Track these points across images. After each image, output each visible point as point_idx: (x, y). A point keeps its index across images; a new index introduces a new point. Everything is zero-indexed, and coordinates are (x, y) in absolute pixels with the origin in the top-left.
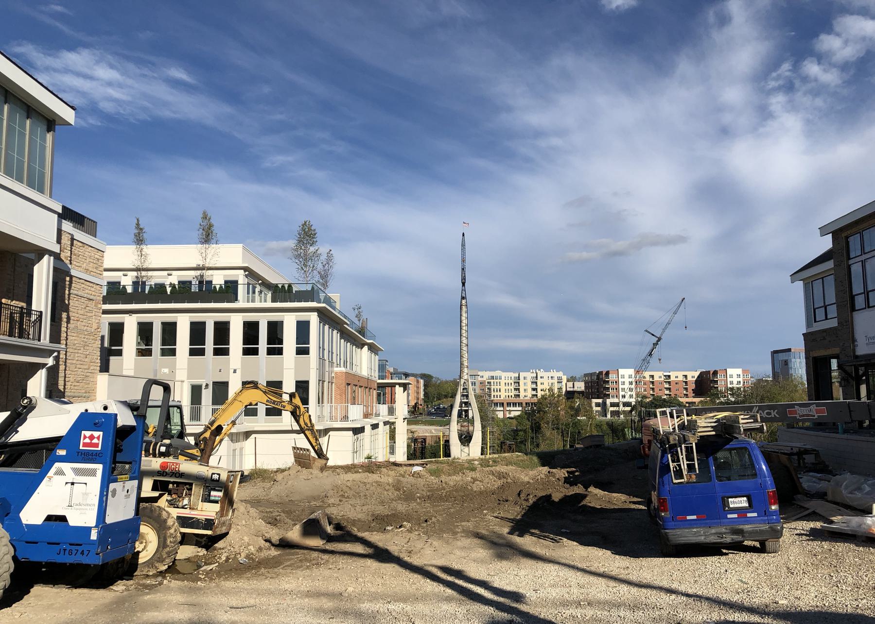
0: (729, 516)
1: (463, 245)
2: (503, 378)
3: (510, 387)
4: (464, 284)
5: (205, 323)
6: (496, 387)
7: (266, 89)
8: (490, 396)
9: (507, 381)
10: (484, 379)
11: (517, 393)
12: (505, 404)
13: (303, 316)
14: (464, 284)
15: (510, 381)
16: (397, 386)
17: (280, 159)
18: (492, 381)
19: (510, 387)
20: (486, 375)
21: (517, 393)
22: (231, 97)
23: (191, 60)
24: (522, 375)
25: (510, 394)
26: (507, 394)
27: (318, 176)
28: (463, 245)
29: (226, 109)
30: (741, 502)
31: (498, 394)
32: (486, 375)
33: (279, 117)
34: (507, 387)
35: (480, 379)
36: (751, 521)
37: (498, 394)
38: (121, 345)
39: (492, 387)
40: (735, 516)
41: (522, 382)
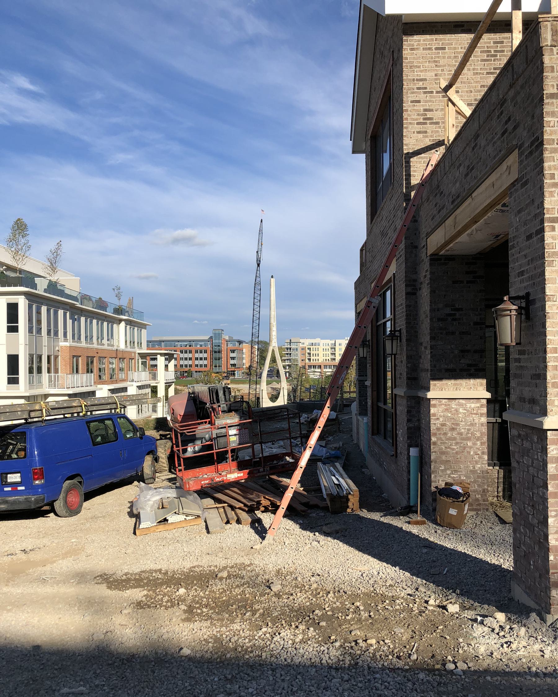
0: (6, 489)
1: (261, 231)
2: (321, 345)
3: (327, 352)
4: (258, 265)
5: (17, 304)
6: (314, 352)
7: (98, 96)
8: (310, 360)
9: (325, 347)
10: (305, 345)
11: (333, 357)
12: (322, 367)
13: (12, 299)
14: (258, 265)
15: (327, 347)
16: (159, 356)
17: (121, 157)
18: (311, 347)
19: (327, 352)
20: (306, 342)
21: (333, 357)
22: (69, 102)
23: (38, 73)
24: (338, 342)
25: (327, 358)
26: (325, 358)
27: (156, 172)
28: (261, 231)
29: (72, 116)
30: (14, 478)
31: (317, 358)
32: (306, 342)
33: (114, 120)
34: (325, 353)
35: (301, 345)
36: (21, 493)
37: (317, 358)
38: (18, 323)
39: (312, 352)
40: (10, 489)
41: (337, 347)
